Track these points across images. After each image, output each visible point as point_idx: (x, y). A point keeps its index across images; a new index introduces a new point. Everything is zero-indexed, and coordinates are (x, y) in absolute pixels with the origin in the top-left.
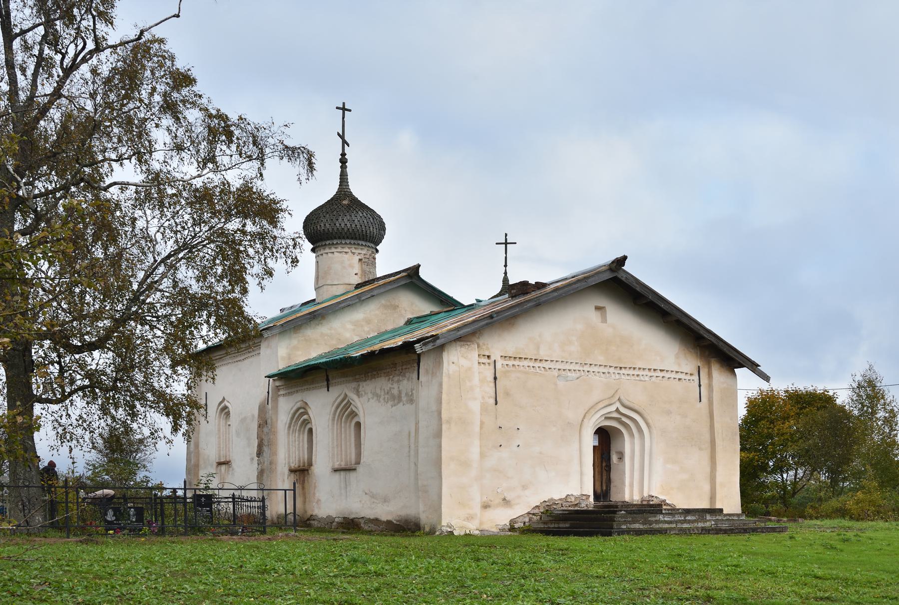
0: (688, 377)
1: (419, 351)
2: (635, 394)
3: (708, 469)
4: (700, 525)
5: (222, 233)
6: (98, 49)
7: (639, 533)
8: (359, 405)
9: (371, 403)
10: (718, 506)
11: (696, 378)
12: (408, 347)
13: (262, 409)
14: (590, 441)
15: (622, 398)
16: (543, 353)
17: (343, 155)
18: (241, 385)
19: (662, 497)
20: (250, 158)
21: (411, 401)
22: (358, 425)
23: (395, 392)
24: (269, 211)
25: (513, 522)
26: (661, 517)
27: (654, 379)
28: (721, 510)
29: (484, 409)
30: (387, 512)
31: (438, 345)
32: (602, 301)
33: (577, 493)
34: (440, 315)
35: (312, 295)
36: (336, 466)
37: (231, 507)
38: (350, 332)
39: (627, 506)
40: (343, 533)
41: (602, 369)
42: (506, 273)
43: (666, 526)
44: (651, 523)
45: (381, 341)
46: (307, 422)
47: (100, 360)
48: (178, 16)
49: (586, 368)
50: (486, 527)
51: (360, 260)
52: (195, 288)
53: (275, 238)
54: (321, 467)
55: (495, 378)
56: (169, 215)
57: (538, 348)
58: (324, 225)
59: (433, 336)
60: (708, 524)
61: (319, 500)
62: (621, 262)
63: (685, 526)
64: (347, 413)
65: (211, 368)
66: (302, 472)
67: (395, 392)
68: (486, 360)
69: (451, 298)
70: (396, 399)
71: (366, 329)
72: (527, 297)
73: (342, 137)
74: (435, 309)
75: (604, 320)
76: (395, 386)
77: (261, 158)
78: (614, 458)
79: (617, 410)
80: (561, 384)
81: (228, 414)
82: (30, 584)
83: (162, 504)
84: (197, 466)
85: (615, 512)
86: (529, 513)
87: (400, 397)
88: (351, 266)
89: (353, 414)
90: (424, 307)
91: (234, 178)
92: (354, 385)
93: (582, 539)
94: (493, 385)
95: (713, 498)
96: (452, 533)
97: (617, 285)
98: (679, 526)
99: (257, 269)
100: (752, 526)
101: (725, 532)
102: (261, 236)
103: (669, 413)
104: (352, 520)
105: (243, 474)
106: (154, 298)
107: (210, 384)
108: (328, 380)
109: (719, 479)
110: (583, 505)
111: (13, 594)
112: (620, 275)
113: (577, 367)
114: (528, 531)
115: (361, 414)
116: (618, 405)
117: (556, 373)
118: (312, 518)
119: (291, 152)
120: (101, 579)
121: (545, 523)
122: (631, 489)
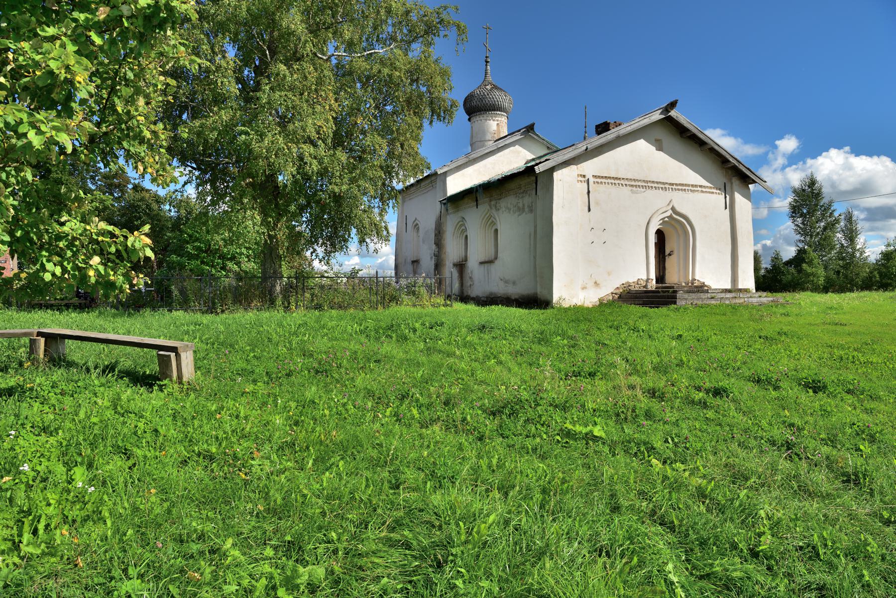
22: (496, 231)
54: (473, 264)
66: (461, 266)
76: (520, 201)
81: (418, 229)
87: (523, 208)
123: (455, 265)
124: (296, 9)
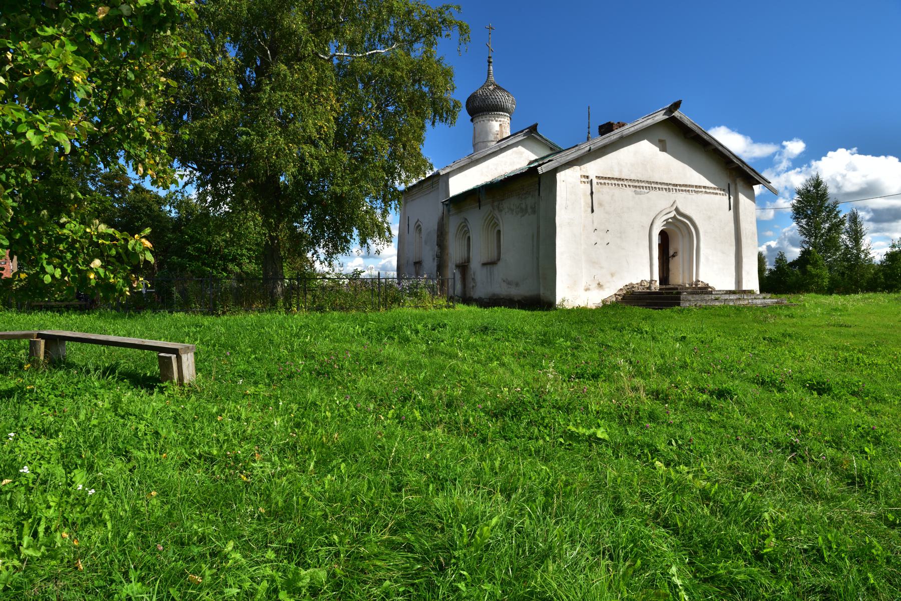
22: (499, 232)
23: (523, 206)
36: (485, 260)
44: (707, 301)
54: (475, 265)
55: (592, 193)
67: (523, 206)
68: (586, 180)
81: (420, 230)
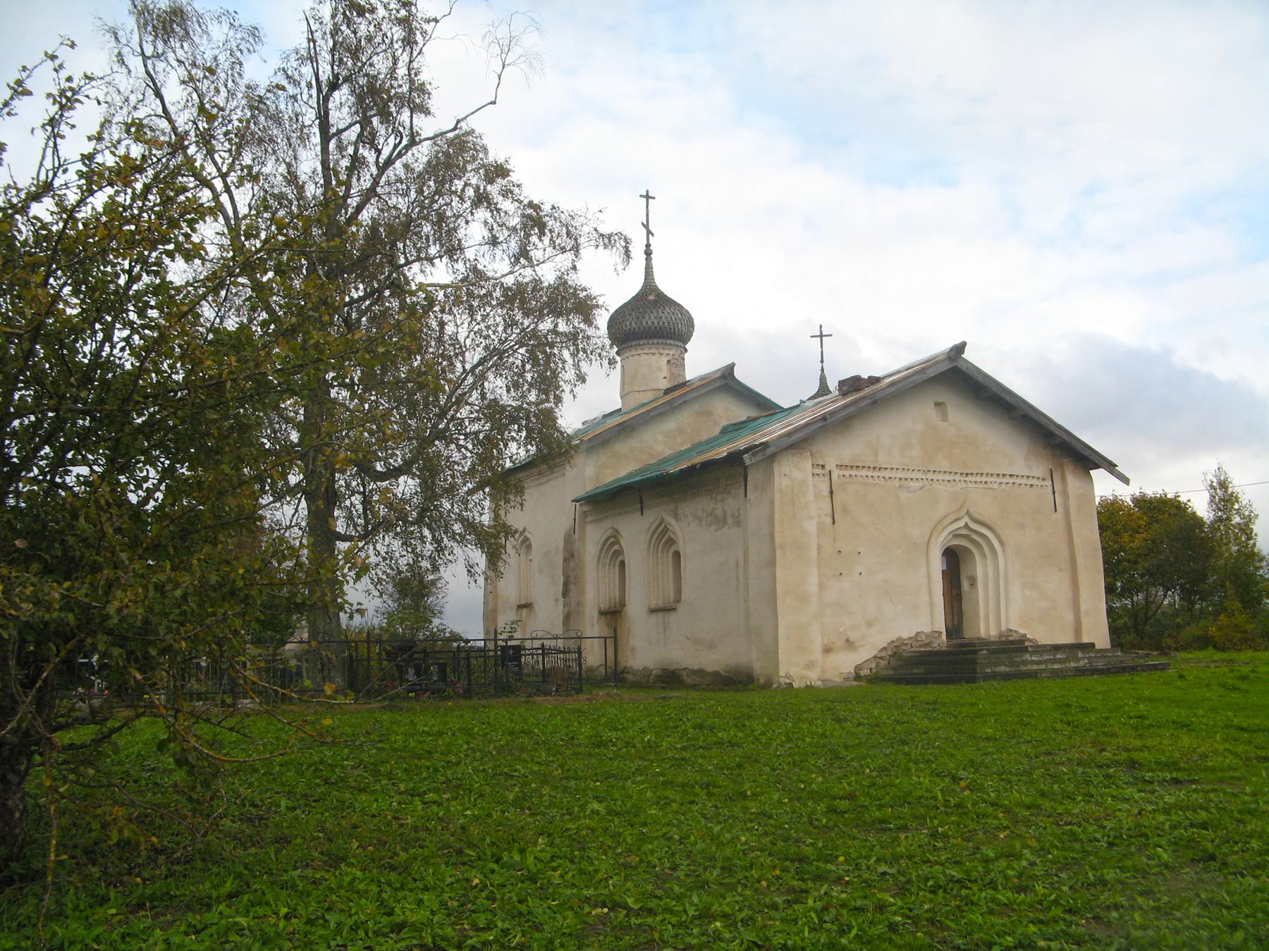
0: (1040, 483)
1: (748, 462)
2: (985, 507)
3: (1070, 595)
4: (1073, 665)
5: (534, 334)
6: (413, 143)
7: (1006, 677)
8: (678, 530)
9: (692, 528)
10: (1085, 640)
11: (1048, 483)
12: (735, 459)
13: (568, 540)
14: (937, 565)
15: (971, 511)
16: (882, 460)
17: (648, 246)
18: (545, 512)
19: (1023, 631)
20: (563, 250)
21: (738, 523)
22: (677, 555)
23: (719, 513)
24: (584, 307)
25: (858, 668)
26: (1028, 657)
27: (1003, 486)
28: (1093, 645)
29: (821, 530)
30: (713, 660)
31: (768, 454)
32: (942, 395)
33: (927, 630)
34: (759, 421)
35: (617, 404)
36: (653, 606)
37: (540, 658)
38: (662, 445)
39: (985, 643)
40: (663, 688)
41: (947, 477)
42: (822, 370)
43: (1035, 667)
45: (699, 453)
46: (619, 553)
47: (407, 486)
48: (494, 103)
49: (930, 476)
50: (828, 676)
51: (668, 361)
52: (507, 400)
53: (589, 338)
54: (636, 608)
56: (479, 318)
57: (876, 455)
58: (630, 324)
59: (761, 444)
60: (1082, 663)
61: (633, 649)
62: (960, 349)
63: (1056, 666)
64: (664, 540)
65: (520, 491)
66: (613, 614)
67: (719, 513)
68: (819, 471)
69: (769, 401)
70: (720, 522)
71: (679, 440)
72: (861, 394)
73: (646, 226)
74: (753, 413)
75: (945, 418)
76: (719, 506)
77: (576, 249)
78: (965, 585)
79: (966, 526)
80: (903, 495)
81: (529, 547)
82: (343, 767)
83: (468, 658)
84: (495, 611)
85: (975, 652)
86: (875, 657)
87: (724, 518)
88: (660, 369)
89: (671, 542)
90: (740, 412)
91: (548, 275)
92: (671, 506)
93: (944, 688)
94: (828, 500)
95: (1078, 630)
96: (791, 684)
97: (955, 378)
98: (1050, 666)
99: (570, 374)
100: (1130, 663)
101: (1102, 672)
102: (573, 337)
103: (1022, 526)
104: (673, 672)
105: (546, 621)
106: (464, 412)
107: (518, 510)
108: (641, 502)
109: (1083, 606)
110: (935, 645)
111: (326, 781)
112: (960, 364)
113: (920, 476)
114: (875, 679)
115: (680, 541)
116: (966, 519)
117: (897, 483)
118: (626, 670)
119: (607, 240)
120: (420, 758)
121: (894, 669)
122: (987, 624)
123: (603, 613)
124: (416, 267)
